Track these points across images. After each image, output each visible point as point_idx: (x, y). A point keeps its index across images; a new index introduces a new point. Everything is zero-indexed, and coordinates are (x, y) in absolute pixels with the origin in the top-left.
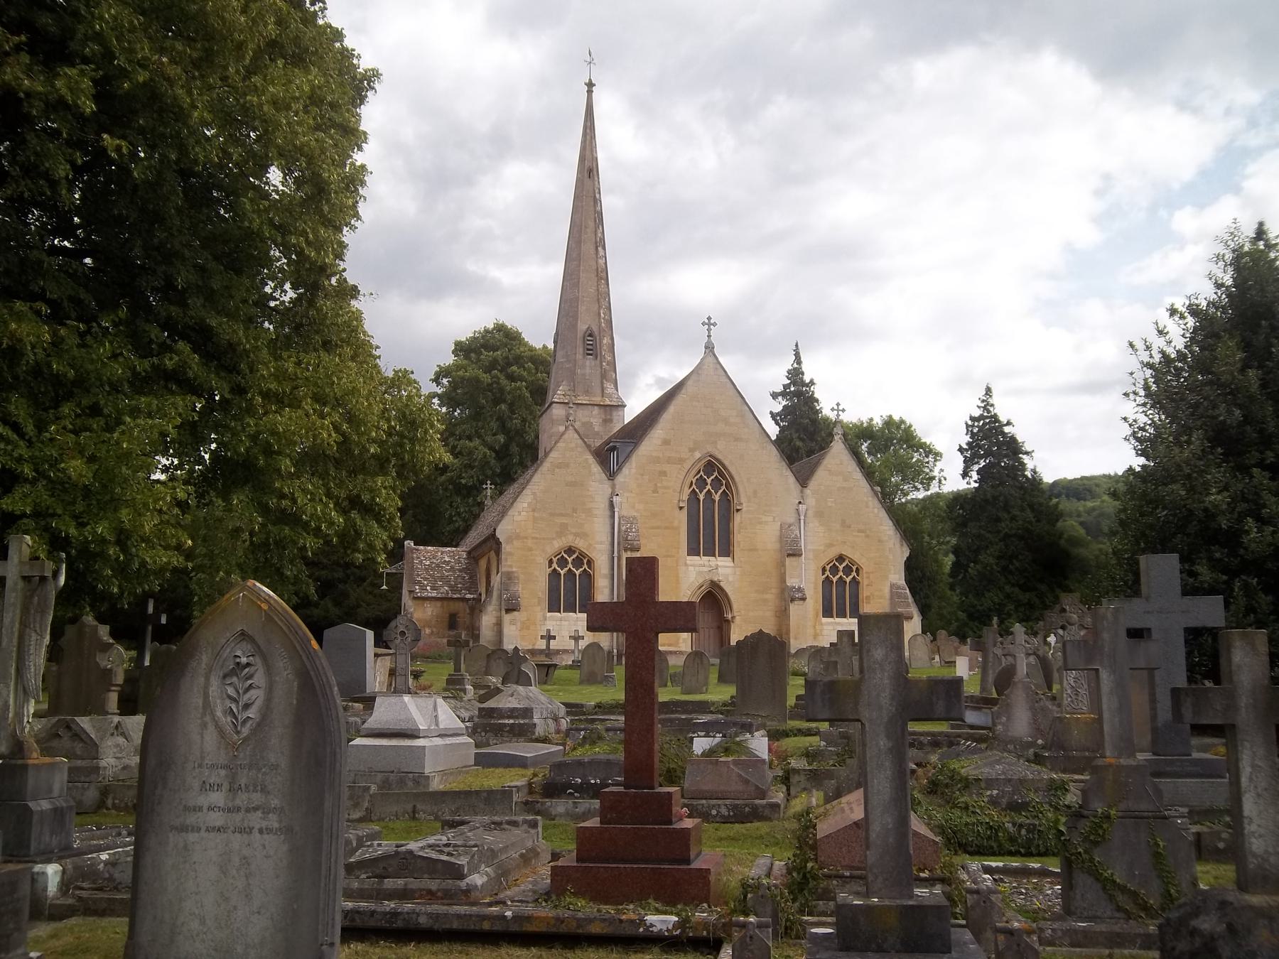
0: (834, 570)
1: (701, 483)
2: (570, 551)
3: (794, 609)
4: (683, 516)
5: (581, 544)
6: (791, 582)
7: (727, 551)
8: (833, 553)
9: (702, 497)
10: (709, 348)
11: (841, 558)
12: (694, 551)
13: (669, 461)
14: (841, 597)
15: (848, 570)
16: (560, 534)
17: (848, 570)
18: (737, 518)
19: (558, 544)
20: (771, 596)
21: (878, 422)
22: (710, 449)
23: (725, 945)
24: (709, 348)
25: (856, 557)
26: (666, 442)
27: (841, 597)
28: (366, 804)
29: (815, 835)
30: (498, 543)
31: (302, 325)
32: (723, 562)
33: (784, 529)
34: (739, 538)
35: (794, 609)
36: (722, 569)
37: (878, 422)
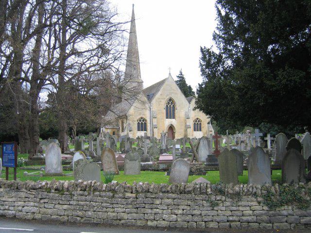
0: (196, 121)
1: (169, 103)
2: (142, 118)
3: (188, 130)
4: (165, 111)
5: (144, 116)
6: (188, 124)
7: (174, 118)
8: (196, 118)
9: (169, 106)
10: (170, 74)
11: (197, 119)
12: (167, 118)
13: (162, 99)
14: (197, 127)
15: (199, 121)
16: (140, 115)
17: (199, 121)
18: (176, 111)
19: (139, 117)
20: (183, 127)
21: (202, 112)
22: (170, 96)
23: (208, 128)
24: (170, 74)
25: (202, 119)
26: (161, 95)
27: (197, 127)
28: (66, 184)
29: (217, 55)
30: (127, 117)
31: (255, 193)
32: (173, 120)
33: (186, 112)
34: (177, 115)
35: (188, 130)
36: (173, 121)
37: (202, 112)
